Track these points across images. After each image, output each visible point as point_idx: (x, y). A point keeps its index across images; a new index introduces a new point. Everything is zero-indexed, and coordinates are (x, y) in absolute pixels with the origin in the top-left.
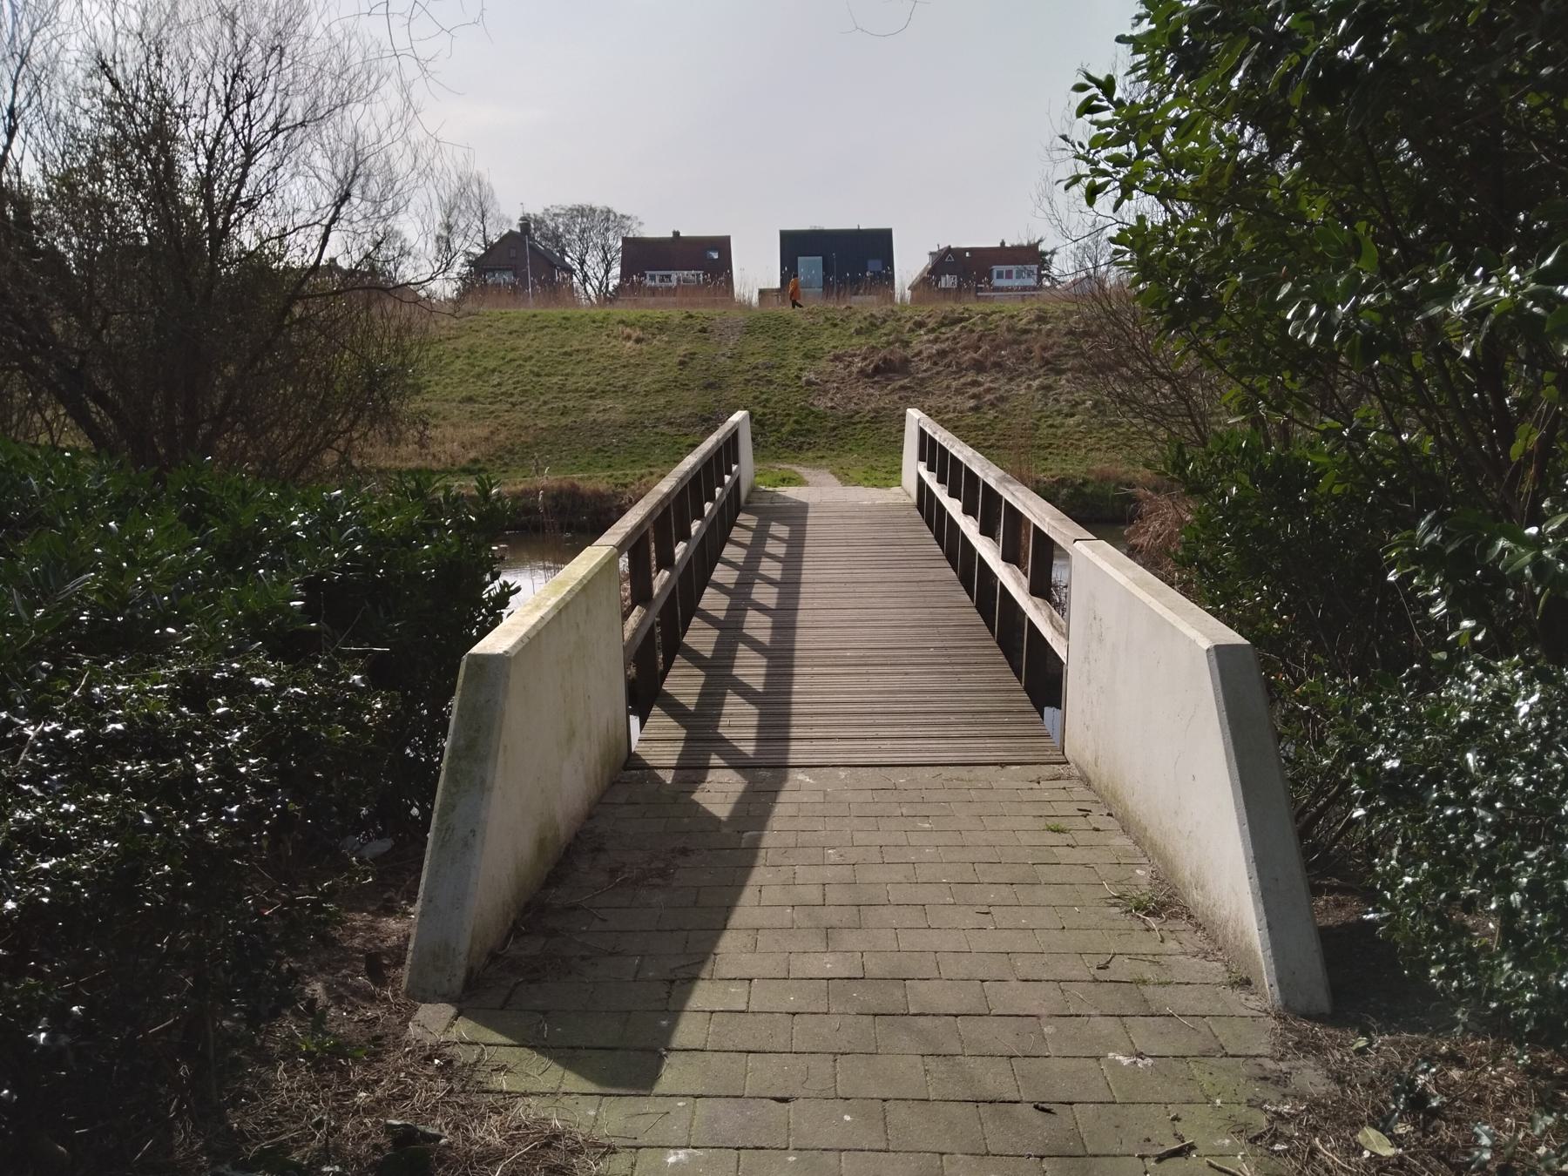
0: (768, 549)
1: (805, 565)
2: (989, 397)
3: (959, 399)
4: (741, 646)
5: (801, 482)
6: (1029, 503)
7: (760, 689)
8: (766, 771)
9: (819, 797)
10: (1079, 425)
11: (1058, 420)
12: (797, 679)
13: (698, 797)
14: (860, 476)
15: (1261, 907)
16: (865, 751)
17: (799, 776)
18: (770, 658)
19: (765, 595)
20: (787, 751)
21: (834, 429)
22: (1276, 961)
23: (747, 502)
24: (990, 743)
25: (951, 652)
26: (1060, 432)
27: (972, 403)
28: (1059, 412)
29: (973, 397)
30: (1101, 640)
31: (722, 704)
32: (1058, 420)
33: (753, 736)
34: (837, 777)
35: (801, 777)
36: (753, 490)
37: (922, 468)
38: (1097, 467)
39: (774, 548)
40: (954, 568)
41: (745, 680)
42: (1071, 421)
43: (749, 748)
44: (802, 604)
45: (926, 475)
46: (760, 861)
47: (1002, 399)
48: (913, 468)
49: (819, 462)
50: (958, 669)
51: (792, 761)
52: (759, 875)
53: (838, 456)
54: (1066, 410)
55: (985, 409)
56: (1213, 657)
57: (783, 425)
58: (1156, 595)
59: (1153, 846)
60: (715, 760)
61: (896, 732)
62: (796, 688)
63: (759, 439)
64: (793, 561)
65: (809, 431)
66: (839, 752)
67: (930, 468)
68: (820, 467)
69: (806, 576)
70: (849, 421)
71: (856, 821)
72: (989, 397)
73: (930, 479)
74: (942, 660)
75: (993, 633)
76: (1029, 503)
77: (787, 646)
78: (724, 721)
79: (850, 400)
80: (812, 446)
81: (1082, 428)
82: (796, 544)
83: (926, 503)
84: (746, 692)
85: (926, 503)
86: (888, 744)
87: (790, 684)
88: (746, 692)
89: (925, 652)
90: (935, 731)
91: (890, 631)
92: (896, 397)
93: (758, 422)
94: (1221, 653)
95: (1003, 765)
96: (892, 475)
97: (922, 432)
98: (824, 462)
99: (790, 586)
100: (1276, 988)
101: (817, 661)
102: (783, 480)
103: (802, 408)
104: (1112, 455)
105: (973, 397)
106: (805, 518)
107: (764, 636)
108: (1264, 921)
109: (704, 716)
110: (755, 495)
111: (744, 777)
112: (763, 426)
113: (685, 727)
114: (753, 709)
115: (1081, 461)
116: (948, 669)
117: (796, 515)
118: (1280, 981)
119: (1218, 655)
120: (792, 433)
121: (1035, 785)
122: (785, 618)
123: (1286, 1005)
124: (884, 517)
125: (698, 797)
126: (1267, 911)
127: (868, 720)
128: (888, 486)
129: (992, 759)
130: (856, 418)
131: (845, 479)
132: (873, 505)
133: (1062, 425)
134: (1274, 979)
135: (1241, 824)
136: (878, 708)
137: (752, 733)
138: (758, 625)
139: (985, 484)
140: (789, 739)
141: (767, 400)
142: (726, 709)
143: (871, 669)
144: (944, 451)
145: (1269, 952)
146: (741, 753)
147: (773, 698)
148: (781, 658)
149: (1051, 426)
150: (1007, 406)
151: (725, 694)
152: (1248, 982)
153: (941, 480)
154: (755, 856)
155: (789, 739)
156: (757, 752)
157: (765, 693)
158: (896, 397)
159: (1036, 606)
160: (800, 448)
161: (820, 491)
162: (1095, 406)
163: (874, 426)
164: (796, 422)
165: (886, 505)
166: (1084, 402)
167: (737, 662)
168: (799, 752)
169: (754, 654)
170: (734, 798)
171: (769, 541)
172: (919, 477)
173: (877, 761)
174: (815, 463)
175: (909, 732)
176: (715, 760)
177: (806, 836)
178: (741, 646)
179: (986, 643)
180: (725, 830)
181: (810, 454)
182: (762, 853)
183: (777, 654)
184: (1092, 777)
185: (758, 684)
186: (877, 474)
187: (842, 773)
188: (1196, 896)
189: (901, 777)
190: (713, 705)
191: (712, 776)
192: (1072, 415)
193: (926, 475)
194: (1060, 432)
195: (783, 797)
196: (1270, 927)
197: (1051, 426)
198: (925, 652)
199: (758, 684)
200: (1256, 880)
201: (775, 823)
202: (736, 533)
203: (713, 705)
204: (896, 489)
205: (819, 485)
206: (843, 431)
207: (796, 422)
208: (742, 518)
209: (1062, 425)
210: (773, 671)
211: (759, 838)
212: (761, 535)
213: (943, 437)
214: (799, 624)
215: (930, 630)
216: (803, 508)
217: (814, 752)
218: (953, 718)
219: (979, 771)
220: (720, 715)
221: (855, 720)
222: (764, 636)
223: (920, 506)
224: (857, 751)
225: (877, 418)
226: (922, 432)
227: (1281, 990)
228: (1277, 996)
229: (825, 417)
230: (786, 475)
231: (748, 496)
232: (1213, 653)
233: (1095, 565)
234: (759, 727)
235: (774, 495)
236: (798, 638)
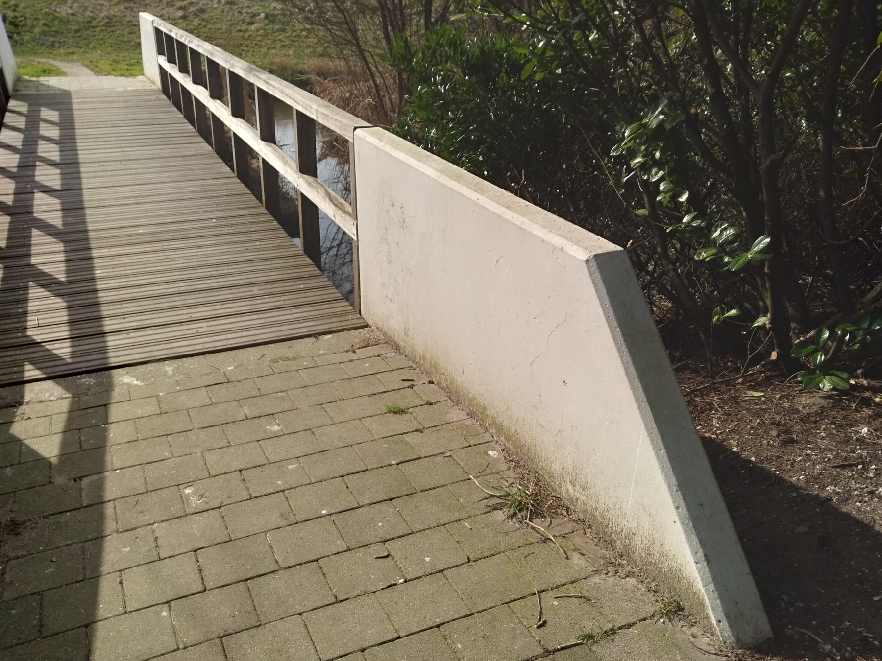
0: (43, 132)
1: (80, 146)
2: (191, 9)
3: (171, 10)
4: (35, 232)
5: (59, 73)
6: (287, 91)
7: (62, 278)
8: (87, 373)
9: (153, 408)
10: (258, 30)
11: (244, 27)
12: (97, 263)
13: (18, 429)
14: (108, 68)
15: (695, 540)
16: (185, 338)
17: (124, 379)
18: (65, 242)
19: (48, 151)
20: (104, 350)
21: (77, 31)
22: (721, 596)
23: (15, 90)
24: (297, 313)
25: (233, 221)
26: (247, 35)
27: (180, 13)
28: (243, 21)
29: (181, 8)
30: (403, 225)
31: (26, 300)
32: (244, 27)
33: (66, 334)
34: (165, 374)
35: (127, 379)
36: (18, 80)
37: (163, 61)
38: (277, 60)
39: (46, 130)
40: (209, 143)
41: (46, 269)
42: (253, 27)
43: (63, 350)
44: (86, 182)
45: (167, 66)
46: (110, 525)
47: (202, 11)
48: (153, 61)
49: (70, 57)
50: (242, 238)
51: (113, 362)
52: (115, 551)
53: (85, 52)
54: (248, 19)
55: (191, 17)
56: (594, 268)
57: (34, 27)
58: (482, 192)
59: (494, 423)
60: (31, 372)
61: (207, 311)
62: (98, 273)
63: (15, 37)
64: (67, 140)
65: (57, 32)
66: (157, 343)
67: (171, 60)
68: (72, 61)
69: (82, 156)
70: (89, 24)
71: (202, 434)
72: (191, 9)
73: (173, 70)
74: (226, 230)
75: (259, 198)
76: (287, 91)
77: (79, 227)
78: (32, 321)
79: (86, 8)
80: (62, 44)
81: (261, 32)
82: (67, 125)
83: (169, 85)
84: (48, 283)
85: (169, 85)
86: (204, 327)
87: (92, 269)
88: (48, 283)
89: (208, 224)
90: (244, 306)
91: (172, 205)
92: (122, 7)
93: (11, 23)
94: (601, 260)
95: (316, 335)
96: (134, 66)
97: (158, 32)
98: (75, 57)
99: (69, 165)
100: (725, 624)
101: (112, 242)
102: (44, 71)
103: (47, 14)
104: (284, 52)
105: (181, 8)
106: (71, 103)
107: (55, 219)
108: (701, 554)
109: (13, 290)
110: (19, 83)
111: (67, 389)
112: (16, 26)
113: (9, 215)
114: (59, 302)
115: (265, 55)
116: (234, 238)
117: (61, 101)
118: (728, 616)
119: (600, 266)
120: (44, 33)
121: (352, 356)
122: (71, 198)
123: (738, 640)
124: (136, 101)
125: (18, 429)
126: (702, 543)
127: (177, 301)
128: (133, 76)
129: (305, 331)
130: (94, 23)
131: (98, 71)
132: (126, 91)
133: (247, 30)
134: (721, 616)
135: (657, 450)
136: (184, 286)
137: (64, 332)
138: (47, 208)
139: (232, 74)
140: (103, 334)
141: (16, 6)
142: (32, 306)
143: (166, 245)
144: (182, 46)
145: (712, 587)
146: (56, 358)
147: (77, 288)
148: (76, 239)
149: (240, 31)
150: (206, 16)
151: (27, 288)
152: (678, 609)
153: (183, 70)
154: (101, 518)
155: (103, 334)
156: (74, 354)
157: (69, 282)
158: (122, 7)
159: (310, 184)
160: (53, 45)
161: (76, 80)
162: (267, 17)
163: (109, 29)
164: (45, 25)
165: (137, 91)
166: (259, 14)
167: (34, 250)
168: (118, 348)
169: (49, 239)
170: (59, 424)
171: (42, 125)
172: (161, 68)
173: (199, 348)
174: (69, 56)
175: (220, 309)
176: (31, 372)
177: (153, 472)
178: (35, 232)
179: (259, 211)
180: (59, 480)
181: (62, 51)
182: (109, 510)
183: (72, 237)
184: (402, 344)
185: (59, 272)
186: (120, 66)
187: (169, 368)
188: (568, 490)
189: (228, 364)
190: (17, 302)
191: (31, 392)
192: (252, 23)
193: (167, 66)
194: (247, 35)
195: (116, 412)
196: (708, 559)
197: (240, 31)
198: (208, 224)
199: (59, 272)
200: (684, 509)
201: (115, 457)
202: (8, 118)
203: (17, 302)
204: (140, 78)
205: (76, 75)
206: (85, 33)
207: (45, 25)
208: (12, 104)
209: (247, 30)
210: (74, 255)
211: (99, 487)
212: (33, 120)
213: (178, 34)
214: (86, 204)
215: (204, 202)
216: (67, 94)
217: (133, 346)
218: (255, 290)
219: (299, 345)
220: (25, 314)
221: (165, 303)
222: (55, 219)
223: (165, 90)
224: (176, 339)
225: (110, 23)
226: (158, 32)
227: (731, 626)
228: (728, 633)
229: (68, 21)
230: (45, 67)
231: (15, 85)
232: (593, 264)
233: (378, 150)
234: (71, 322)
235: (38, 85)
236: (89, 219)
